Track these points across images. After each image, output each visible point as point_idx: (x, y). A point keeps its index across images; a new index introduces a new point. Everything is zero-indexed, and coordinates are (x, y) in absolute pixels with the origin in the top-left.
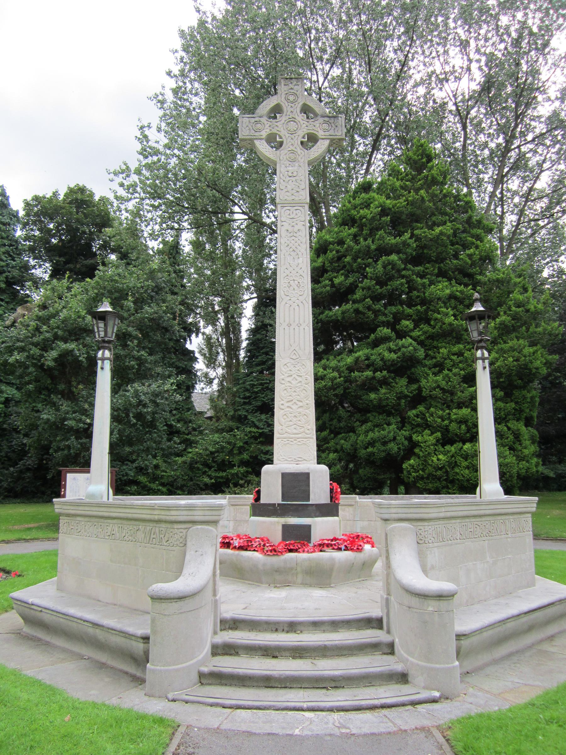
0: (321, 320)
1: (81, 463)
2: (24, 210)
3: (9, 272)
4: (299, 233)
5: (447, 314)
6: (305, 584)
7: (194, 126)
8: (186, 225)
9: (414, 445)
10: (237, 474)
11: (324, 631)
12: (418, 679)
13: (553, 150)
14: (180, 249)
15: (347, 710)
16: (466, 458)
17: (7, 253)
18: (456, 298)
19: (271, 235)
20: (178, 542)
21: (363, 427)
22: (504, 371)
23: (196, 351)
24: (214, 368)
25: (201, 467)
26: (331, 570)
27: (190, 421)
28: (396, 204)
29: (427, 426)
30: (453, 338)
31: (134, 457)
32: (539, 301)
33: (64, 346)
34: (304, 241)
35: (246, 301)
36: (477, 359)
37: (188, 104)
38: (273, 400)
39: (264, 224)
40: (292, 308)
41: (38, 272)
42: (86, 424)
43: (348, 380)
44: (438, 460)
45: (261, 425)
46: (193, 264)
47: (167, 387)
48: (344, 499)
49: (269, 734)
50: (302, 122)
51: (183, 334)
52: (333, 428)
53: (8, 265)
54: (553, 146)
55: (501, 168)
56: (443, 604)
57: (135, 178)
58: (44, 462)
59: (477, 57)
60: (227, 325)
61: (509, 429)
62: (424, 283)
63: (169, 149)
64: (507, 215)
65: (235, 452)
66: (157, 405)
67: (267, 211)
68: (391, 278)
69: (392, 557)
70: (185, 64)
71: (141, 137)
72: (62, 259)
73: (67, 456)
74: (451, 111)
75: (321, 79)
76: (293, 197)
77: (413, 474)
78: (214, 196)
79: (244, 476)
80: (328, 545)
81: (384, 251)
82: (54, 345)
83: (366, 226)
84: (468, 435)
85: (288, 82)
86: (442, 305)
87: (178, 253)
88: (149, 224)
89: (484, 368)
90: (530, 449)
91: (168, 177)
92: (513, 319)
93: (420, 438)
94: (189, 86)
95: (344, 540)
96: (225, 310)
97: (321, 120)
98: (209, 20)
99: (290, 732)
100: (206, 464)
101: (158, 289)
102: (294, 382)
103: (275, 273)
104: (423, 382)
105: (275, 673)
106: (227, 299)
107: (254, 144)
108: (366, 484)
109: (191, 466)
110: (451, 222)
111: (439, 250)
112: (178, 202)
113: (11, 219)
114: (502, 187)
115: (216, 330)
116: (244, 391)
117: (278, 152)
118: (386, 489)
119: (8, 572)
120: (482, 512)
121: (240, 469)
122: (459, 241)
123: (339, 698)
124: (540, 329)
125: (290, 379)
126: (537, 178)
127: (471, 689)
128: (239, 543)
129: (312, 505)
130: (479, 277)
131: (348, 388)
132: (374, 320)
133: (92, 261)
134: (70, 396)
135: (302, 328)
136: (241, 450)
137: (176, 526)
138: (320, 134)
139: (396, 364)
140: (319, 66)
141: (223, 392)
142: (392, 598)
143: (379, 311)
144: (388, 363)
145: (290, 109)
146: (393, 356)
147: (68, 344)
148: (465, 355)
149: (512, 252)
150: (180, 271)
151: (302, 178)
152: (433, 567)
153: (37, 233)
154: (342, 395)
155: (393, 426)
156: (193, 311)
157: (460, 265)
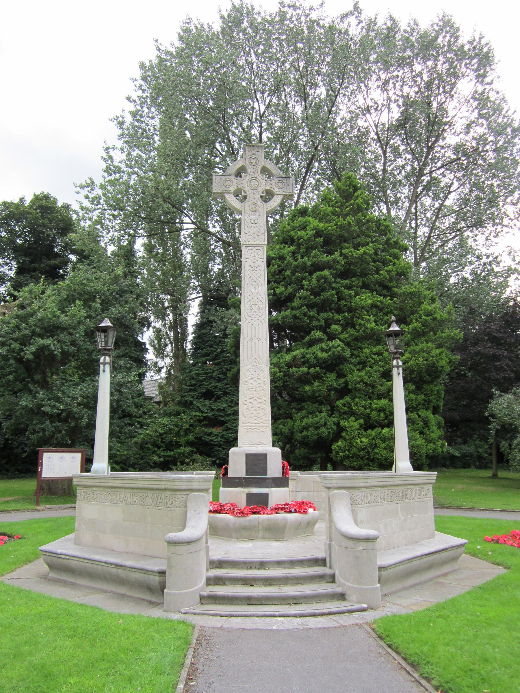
1: (53, 444)
6: (264, 538)
10: (183, 454)
11: (285, 568)
15: (306, 616)
16: (384, 440)
18: (376, 307)
21: (299, 414)
22: (415, 369)
24: (163, 358)
25: (150, 447)
26: (285, 527)
27: (141, 406)
29: (352, 413)
30: (374, 340)
36: (393, 367)
39: (210, 233)
40: (253, 326)
42: (60, 410)
43: (286, 374)
44: (361, 442)
45: (205, 410)
47: (131, 379)
48: (293, 474)
50: (262, 181)
55: (416, 188)
56: (369, 545)
57: (98, 192)
58: (10, 442)
60: (175, 320)
61: (419, 416)
65: (182, 434)
67: (213, 222)
68: (323, 290)
70: (144, 91)
72: (27, 259)
73: (41, 437)
74: (373, 139)
77: (341, 454)
79: (189, 455)
80: (282, 509)
81: (317, 267)
82: (32, 340)
84: (386, 421)
86: (365, 313)
88: (109, 232)
89: (399, 374)
90: (436, 433)
91: (128, 192)
92: (423, 326)
93: (346, 424)
96: (174, 308)
97: (276, 180)
100: (155, 445)
104: (350, 377)
109: (142, 446)
110: (372, 242)
111: (363, 267)
112: (136, 214)
116: (190, 379)
117: (243, 204)
119: (9, 536)
120: (396, 483)
121: (186, 449)
125: (251, 381)
126: (446, 197)
129: (270, 478)
131: (287, 381)
132: (308, 324)
134: (45, 384)
135: (261, 341)
136: (187, 432)
137: (178, 493)
138: (276, 190)
143: (313, 317)
144: (320, 361)
146: (325, 355)
148: (384, 354)
149: (424, 260)
150: (134, 272)
151: (262, 225)
152: (362, 522)
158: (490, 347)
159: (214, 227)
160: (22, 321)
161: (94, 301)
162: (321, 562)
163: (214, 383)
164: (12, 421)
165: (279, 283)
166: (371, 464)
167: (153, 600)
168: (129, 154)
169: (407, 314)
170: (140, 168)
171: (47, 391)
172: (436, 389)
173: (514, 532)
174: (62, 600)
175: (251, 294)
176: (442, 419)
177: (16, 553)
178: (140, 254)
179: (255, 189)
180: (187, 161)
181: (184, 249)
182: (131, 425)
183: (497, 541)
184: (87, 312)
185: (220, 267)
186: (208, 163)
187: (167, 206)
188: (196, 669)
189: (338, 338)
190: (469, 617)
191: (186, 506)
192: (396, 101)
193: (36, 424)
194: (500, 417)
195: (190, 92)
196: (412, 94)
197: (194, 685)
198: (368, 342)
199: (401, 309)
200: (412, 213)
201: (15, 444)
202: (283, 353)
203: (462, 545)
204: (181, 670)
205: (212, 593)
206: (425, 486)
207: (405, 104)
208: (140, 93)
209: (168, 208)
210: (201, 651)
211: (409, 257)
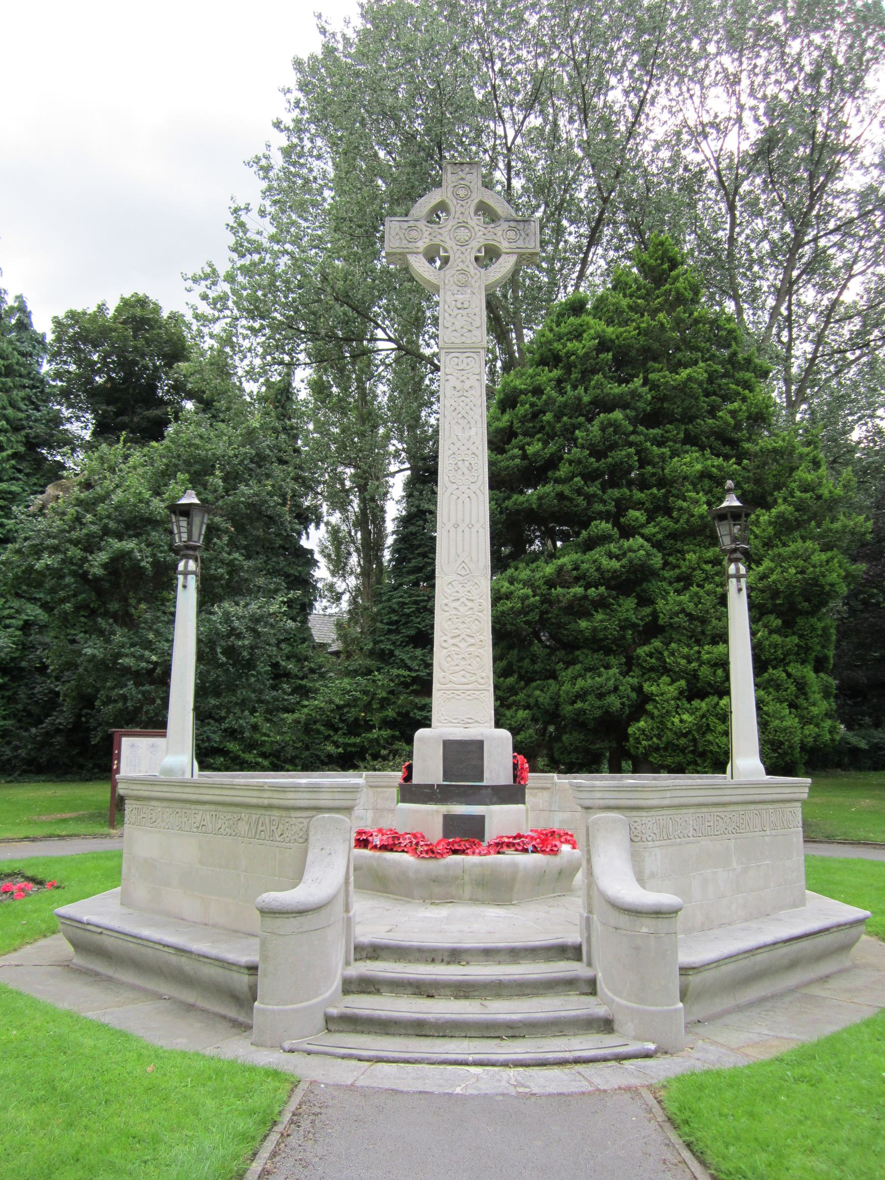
0: (507, 508)
2: (54, 332)
3: (31, 428)
4: (471, 392)
5: (696, 502)
6: (475, 900)
7: (315, 205)
8: (302, 357)
9: (647, 698)
10: (377, 740)
11: (500, 963)
12: (626, 1026)
13: (868, 244)
14: (292, 394)
17: (28, 398)
18: (710, 476)
19: (432, 373)
20: (296, 837)
21: (570, 671)
22: (782, 588)
23: (316, 550)
24: (343, 576)
25: (322, 728)
26: (514, 879)
28: (621, 334)
30: (707, 537)
31: (223, 714)
35: (393, 475)
37: (305, 171)
38: (432, 627)
39: (421, 357)
40: (460, 502)
41: (74, 428)
42: (151, 663)
44: (681, 721)
45: (414, 665)
46: (313, 417)
47: (273, 608)
48: (533, 779)
49: (421, 1092)
50: (477, 228)
51: (297, 527)
52: (523, 672)
53: (28, 417)
54: (869, 238)
55: (788, 270)
56: (662, 924)
57: (224, 287)
58: (83, 719)
59: (752, 102)
60: (363, 511)
61: (789, 675)
62: (663, 453)
63: (278, 242)
64: (797, 342)
66: (257, 634)
67: (426, 337)
68: (613, 447)
69: (594, 860)
70: (303, 110)
71: (235, 225)
72: (111, 408)
73: (121, 710)
74: (711, 184)
75: (511, 133)
76: (464, 339)
78: (345, 314)
80: (509, 845)
81: (605, 405)
82: (103, 543)
83: (576, 367)
85: (457, 169)
86: (690, 487)
87: (289, 399)
88: (245, 357)
89: (740, 590)
90: (820, 706)
91: (274, 286)
92: (797, 510)
93: (654, 689)
94: (308, 144)
95: (532, 838)
96: (362, 488)
97: (505, 225)
98: (340, 47)
99: (450, 1091)
100: (330, 725)
101: (260, 459)
103: (436, 432)
104: (660, 603)
105: (430, 1016)
106: (364, 472)
107: (407, 261)
108: (574, 756)
109: (307, 728)
110: (705, 360)
111: (686, 403)
112: (290, 324)
113: (34, 347)
114: (790, 300)
115: (347, 517)
116: (389, 613)
119: (40, 883)
121: (382, 732)
122: (717, 389)
123: (518, 1050)
124: (837, 525)
125: (456, 604)
127: (700, 1042)
128: (381, 840)
130: (747, 445)
132: (586, 509)
133: (158, 412)
134: (126, 620)
135: (474, 530)
136: (384, 703)
137: (293, 814)
138: (504, 246)
139: (619, 577)
140: (506, 113)
141: (357, 614)
142: (595, 917)
143: (594, 495)
145: (459, 210)
146: (615, 564)
147: (124, 543)
149: (804, 400)
150: (292, 428)
151: (477, 310)
152: (653, 875)
153: (73, 368)
155: (615, 670)
156: (312, 489)
157: (718, 427)
162: (574, 952)
169: (767, 488)
175: (455, 441)
189: (639, 534)
193: (113, 688)
199: (758, 481)
200: (781, 315)
202: (541, 563)
205: (348, 1011)
206: (788, 805)
210: (293, 1141)
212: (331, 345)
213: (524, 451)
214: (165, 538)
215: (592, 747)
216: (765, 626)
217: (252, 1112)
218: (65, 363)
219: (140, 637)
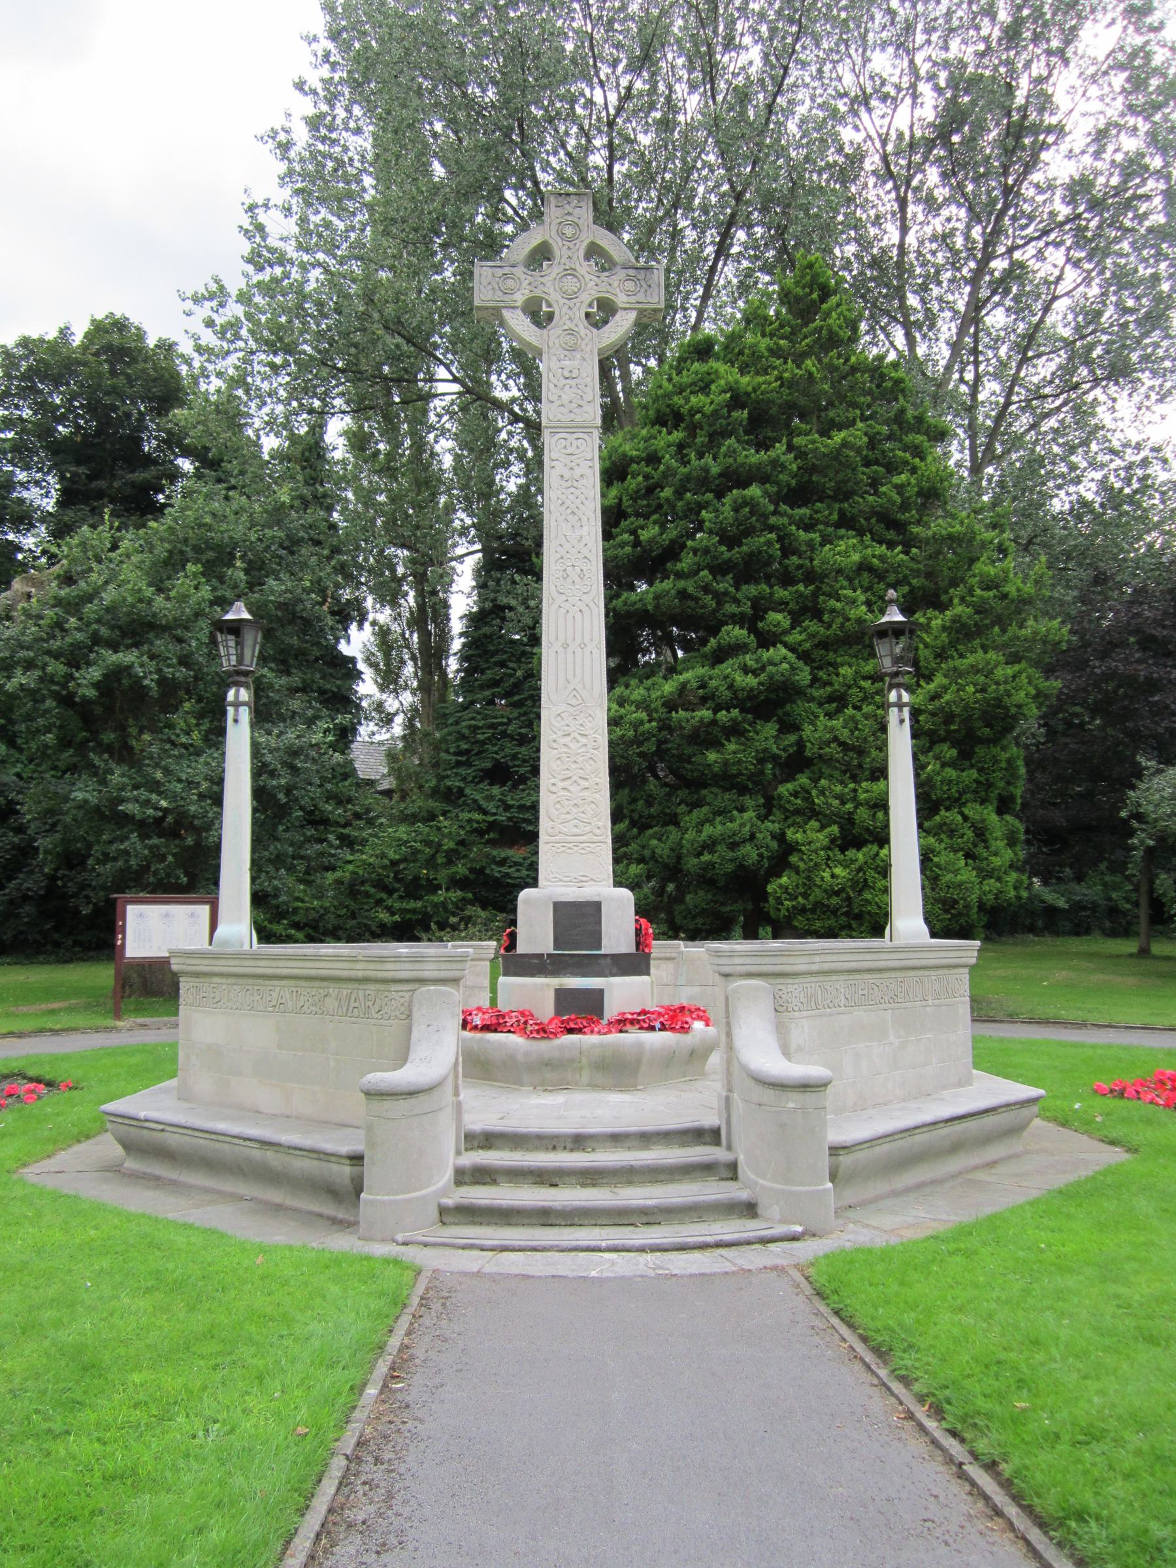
1: (149, 884)
5: (853, 602)
6: (593, 1086)
10: (444, 904)
12: (771, 1210)
15: (666, 1250)
18: (870, 569)
19: (511, 424)
22: (957, 711)
23: (360, 657)
24: (395, 691)
25: (372, 890)
27: (349, 800)
28: (760, 385)
29: (813, 813)
32: (1026, 577)
33: (114, 658)
34: (591, 494)
36: (890, 705)
39: (498, 405)
40: (570, 616)
41: (32, 495)
42: (160, 809)
43: (665, 726)
44: (833, 876)
45: (491, 807)
47: (317, 737)
48: (659, 948)
50: (588, 277)
52: (636, 817)
56: (810, 1098)
57: (236, 310)
58: (60, 883)
60: (421, 607)
61: (966, 818)
62: (812, 540)
63: (307, 251)
66: (294, 769)
67: (503, 377)
68: (749, 532)
70: (334, 66)
72: (81, 470)
73: (121, 870)
76: (572, 416)
80: (632, 1022)
81: (736, 478)
82: (92, 656)
86: (845, 583)
88: (265, 404)
89: (902, 721)
90: (1003, 856)
91: (303, 309)
92: (977, 612)
93: (799, 836)
95: (660, 1014)
96: (420, 579)
97: (621, 274)
100: (381, 885)
101: (292, 544)
102: (573, 746)
104: (808, 730)
108: (699, 921)
109: (353, 889)
110: (864, 419)
111: (840, 476)
112: (324, 361)
116: (457, 740)
117: (545, 331)
118: (738, 930)
119: (50, 1084)
125: (566, 740)
131: (666, 741)
132: (715, 611)
134: (124, 753)
135: (587, 651)
136: (452, 857)
137: (394, 987)
138: (621, 299)
139: (756, 697)
143: (726, 593)
146: (751, 681)
150: (325, 496)
151: (588, 380)
152: (799, 1049)
154: (654, 754)
155: (750, 814)
158: (1139, 661)
159: (506, 388)
160: (68, 612)
161: (230, 565)
162: (712, 1136)
163: (510, 748)
164: (58, 836)
165: (646, 517)
166: (854, 924)
167: (340, 1216)
168: (304, 220)
170: (328, 252)
171: (131, 767)
172: (1004, 756)
173: (1162, 1073)
174: (143, 1215)
176: (1021, 827)
177: (61, 1119)
178: (338, 455)
179: (571, 297)
180: (438, 234)
181: (436, 442)
182: (321, 841)
183: (1120, 1092)
184: (214, 589)
185: (522, 481)
186: (486, 237)
187: (393, 341)
188: (412, 1358)
190: (1020, 1253)
191: (409, 1016)
192: (932, 77)
193: (110, 842)
194: (1156, 820)
195: (441, 65)
196: (969, 57)
197: (401, 1390)
198: (851, 652)
199: (929, 575)
201: (72, 888)
202: (658, 679)
203: (1033, 1101)
204: (376, 1360)
207: (953, 83)
208: (325, 71)
209: (397, 346)
210: (427, 1321)
211: (957, 454)
212: (377, 387)
213: (637, 537)
214: (174, 648)
215: (722, 909)
216: (937, 758)
217: (382, 1294)
218: (17, 407)
219: (144, 776)
